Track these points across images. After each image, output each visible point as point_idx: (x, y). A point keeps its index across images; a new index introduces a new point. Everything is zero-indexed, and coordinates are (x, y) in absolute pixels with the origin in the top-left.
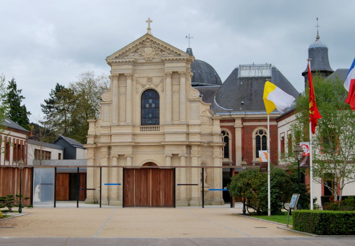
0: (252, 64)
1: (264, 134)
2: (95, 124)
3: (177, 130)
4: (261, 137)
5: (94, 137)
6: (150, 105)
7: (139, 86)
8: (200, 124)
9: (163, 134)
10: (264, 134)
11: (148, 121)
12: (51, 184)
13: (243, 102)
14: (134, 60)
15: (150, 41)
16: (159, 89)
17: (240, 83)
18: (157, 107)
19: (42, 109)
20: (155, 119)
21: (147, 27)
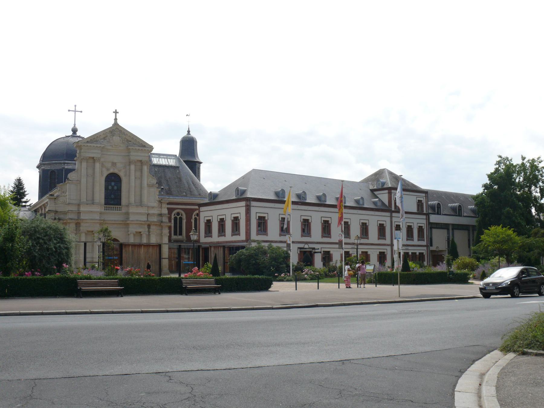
0: (71, 133)
1: (180, 216)
3: (140, 211)
4: (178, 218)
5: (100, 213)
6: (113, 187)
7: (104, 169)
10: (180, 216)
12: (344, 218)
13: (162, 187)
15: (119, 130)
16: (121, 174)
17: (155, 170)
18: (119, 190)
19: (15, 182)
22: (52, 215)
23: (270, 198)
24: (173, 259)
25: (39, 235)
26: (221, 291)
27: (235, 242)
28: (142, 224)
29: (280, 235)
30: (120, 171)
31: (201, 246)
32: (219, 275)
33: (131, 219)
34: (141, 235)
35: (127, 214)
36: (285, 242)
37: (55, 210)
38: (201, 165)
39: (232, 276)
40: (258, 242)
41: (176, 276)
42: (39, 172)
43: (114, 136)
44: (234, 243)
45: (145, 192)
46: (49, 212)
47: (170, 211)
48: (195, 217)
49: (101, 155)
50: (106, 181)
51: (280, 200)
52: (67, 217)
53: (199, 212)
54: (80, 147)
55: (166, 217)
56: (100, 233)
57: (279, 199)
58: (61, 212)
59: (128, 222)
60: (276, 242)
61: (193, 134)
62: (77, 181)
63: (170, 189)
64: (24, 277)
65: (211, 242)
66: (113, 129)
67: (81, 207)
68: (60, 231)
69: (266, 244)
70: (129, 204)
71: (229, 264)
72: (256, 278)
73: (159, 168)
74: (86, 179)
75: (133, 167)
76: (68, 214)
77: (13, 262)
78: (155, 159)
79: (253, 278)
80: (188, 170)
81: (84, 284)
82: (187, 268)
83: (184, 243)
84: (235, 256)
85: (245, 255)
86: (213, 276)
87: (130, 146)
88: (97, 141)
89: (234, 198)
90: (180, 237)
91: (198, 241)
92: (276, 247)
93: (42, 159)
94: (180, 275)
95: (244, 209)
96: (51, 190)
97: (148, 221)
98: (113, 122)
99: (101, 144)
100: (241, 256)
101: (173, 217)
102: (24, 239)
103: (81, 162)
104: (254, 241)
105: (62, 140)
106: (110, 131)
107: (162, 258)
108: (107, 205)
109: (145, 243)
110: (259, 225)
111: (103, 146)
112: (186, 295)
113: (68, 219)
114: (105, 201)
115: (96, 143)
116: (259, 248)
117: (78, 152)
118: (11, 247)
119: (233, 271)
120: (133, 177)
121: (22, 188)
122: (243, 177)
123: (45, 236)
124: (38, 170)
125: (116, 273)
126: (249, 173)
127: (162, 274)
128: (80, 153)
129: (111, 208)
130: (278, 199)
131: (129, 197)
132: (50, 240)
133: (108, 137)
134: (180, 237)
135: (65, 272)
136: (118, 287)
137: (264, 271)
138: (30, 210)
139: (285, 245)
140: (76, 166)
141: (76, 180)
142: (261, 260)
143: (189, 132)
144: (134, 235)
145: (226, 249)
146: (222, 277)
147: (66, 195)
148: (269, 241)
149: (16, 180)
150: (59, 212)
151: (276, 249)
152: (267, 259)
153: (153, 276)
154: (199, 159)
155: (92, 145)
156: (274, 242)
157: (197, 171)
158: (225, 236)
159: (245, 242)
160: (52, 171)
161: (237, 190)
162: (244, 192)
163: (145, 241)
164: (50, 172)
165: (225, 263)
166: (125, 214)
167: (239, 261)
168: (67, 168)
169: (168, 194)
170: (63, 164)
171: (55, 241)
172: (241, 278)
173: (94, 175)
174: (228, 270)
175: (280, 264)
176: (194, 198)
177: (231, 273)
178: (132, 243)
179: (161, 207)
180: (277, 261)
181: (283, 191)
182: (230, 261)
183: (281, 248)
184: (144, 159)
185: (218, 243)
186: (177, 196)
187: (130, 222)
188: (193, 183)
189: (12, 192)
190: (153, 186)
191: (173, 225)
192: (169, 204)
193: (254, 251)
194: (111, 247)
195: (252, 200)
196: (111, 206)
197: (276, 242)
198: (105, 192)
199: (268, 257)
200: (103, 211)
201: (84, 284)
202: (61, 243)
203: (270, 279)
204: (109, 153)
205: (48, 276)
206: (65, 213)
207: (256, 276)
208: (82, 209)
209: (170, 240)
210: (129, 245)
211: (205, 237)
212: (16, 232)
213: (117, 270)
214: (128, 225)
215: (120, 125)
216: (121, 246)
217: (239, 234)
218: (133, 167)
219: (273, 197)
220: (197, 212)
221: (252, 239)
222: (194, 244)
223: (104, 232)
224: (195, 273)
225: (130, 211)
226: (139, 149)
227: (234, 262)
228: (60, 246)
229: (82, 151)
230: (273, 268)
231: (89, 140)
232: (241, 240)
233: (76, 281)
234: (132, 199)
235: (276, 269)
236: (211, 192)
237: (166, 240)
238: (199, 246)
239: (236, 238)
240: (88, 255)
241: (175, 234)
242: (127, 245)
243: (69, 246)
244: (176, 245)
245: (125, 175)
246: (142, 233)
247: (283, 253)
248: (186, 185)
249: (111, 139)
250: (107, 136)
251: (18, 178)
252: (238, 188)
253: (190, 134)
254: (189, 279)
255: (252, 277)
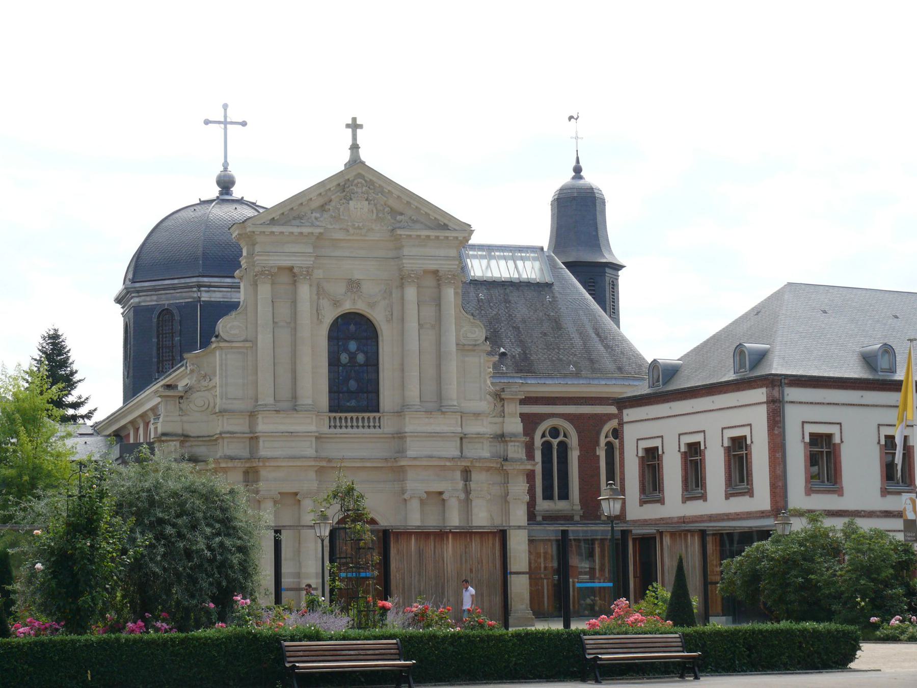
0: (214, 191)
1: (561, 438)
2: (179, 403)
3: (438, 429)
5: (317, 438)
6: (352, 357)
7: (325, 303)
8: (300, 402)
9: (399, 438)
10: (561, 438)
11: (348, 401)
13: (502, 350)
14: (322, 231)
15: (366, 181)
16: (378, 316)
17: (477, 296)
18: (373, 363)
19: (41, 344)
20: (365, 395)
21: (350, 143)
22: (174, 445)
23: (846, 375)
24: (543, 576)
25: (162, 512)
26: (702, 671)
27: (738, 516)
28: (443, 468)
29: (885, 492)
30: (372, 305)
31: (631, 531)
32: (691, 623)
33: (410, 453)
34: (444, 500)
35: (400, 436)
36: (899, 515)
37: (180, 431)
38: (620, 273)
39: (732, 627)
40: (812, 516)
41: (557, 626)
42: (122, 314)
43: (351, 199)
44: (733, 519)
45: (452, 367)
46: (164, 438)
47: (530, 422)
48: (608, 439)
49: (313, 259)
50: (331, 338)
51: (878, 380)
52: (219, 454)
53: (621, 424)
54: (251, 238)
55: (517, 444)
56: (331, 501)
57: (877, 377)
58: (198, 437)
59: (402, 463)
60: (870, 514)
61: (590, 178)
62: (246, 341)
63: (525, 356)
64: (124, 636)
65: (662, 519)
66: (347, 178)
67: (260, 420)
68: (219, 500)
69: (838, 523)
70: (403, 406)
71: (722, 589)
72: (806, 629)
73: (488, 289)
74: (271, 335)
75: (411, 293)
76: (220, 441)
77: (96, 592)
78: (476, 263)
79: (799, 631)
80: (580, 294)
81: (301, 653)
82: (588, 601)
83: (577, 523)
84: (741, 563)
85: (772, 559)
86: (675, 625)
87: (399, 228)
88: (299, 217)
89: (730, 376)
90: (560, 506)
91: (621, 517)
92: (871, 530)
93: (130, 276)
94: (567, 625)
95: (763, 409)
96: (162, 371)
97: (461, 457)
98: (346, 156)
99: (312, 225)
100: (760, 560)
101: (538, 442)
102: (123, 525)
103: (255, 284)
104: (800, 514)
105: (190, 214)
106: (339, 185)
107: (511, 573)
108: (336, 412)
109: (456, 527)
110: (813, 460)
111: (318, 231)
112: (597, 681)
113: (221, 457)
114: (330, 399)
115: (297, 222)
116: (816, 537)
117: (245, 254)
118: (90, 551)
119: (733, 608)
120: (412, 325)
121: (64, 363)
122: (757, 311)
123: (178, 516)
124: (118, 309)
125: (382, 620)
126: (777, 296)
127: (511, 621)
128: (251, 254)
129: (349, 420)
130: (871, 377)
131: (403, 386)
132: (194, 527)
133: (333, 204)
134: (560, 506)
135: (239, 618)
136: (399, 660)
137: (834, 607)
138: (98, 434)
139: (898, 524)
140: (240, 292)
141: (242, 338)
142: (822, 575)
143: (578, 170)
144: (422, 502)
145: (709, 540)
146: (699, 628)
147: (212, 384)
148: (847, 511)
149: (44, 338)
150: (192, 439)
151: (871, 538)
152: (841, 569)
153: (492, 627)
154: (614, 256)
155: (286, 229)
156: (864, 516)
157: (607, 295)
158: (704, 497)
159: (768, 516)
160: (163, 310)
161: (739, 351)
162: (761, 357)
163: (454, 520)
164: (156, 313)
165: (706, 583)
166: (394, 438)
167: (753, 578)
168: (207, 299)
169: (520, 371)
170: (195, 289)
171: (208, 530)
172: (760, 632)
173: (295, 323)
174: (719, 608)
175: (886, 586)
176: (604, 382)
177: (729, 615)
178: (418, 527)
179: (502, 414)
180: (874, 576)
181: (888, 350)
182: (722, 579)
183: (888, 535)
184: (445, 266)
185: (684, 522)
186: (550, 376)
187: (410, 463)
188: (598, 335)
189: (31, 373)
190: (476, 348)
191: (538, 469)
192: (525, 401)
193: (801, 546)
194: (365, 543)
195: (786, 381)
196: (349, 415)
197: (870, 514)
198: (329, 372)
199: (847, 563)
200: (325, 429)
201: (301, 653)
202: (225, 535)
203: (853, 632)
204: (338, 253)
205: (200, 633)
206: (211, 440)
207: (809, 625)
208: (263, 426)
209: (531, 516)
210: (410, 534)
211: (642, 503)
212: (101, 507)
213: (385, 610)
214: (402, 470)
215: (367, 164)
216: (386, 537)
217: (750, 493)
218: (411, 293)
219: (855, 371)
220: (614, 423)
221: (791, 506)
222: (612, 527)
223: (343, 499)
224: (617, 618)
225: (407, 430)
226: (428, 237)
227: (738, 582)
228: (221, 544)
229: (258, 248)
230: (863, 599)
231: (276, 215)
232: (757, 512)
233: (281, 644)
234: (413, 393)
235: (872, 601)
236: (655, 360)
237: (519, 515)
238: (625, 533)
239: (740, 505)
240: (286, 569)
241: (548, 496)
242: (405, 534)
243: (249, 544)
244: (552, 531)
245: (389, 320)
246: (445, 496)
247: (895, 550)
248: (578, 341)
249: (341, 210)
250: (330, 201)
251: (52, 332)
252: (740, 344)
253: (581, 178)
254: (605, 634)
255: (795, 626)
